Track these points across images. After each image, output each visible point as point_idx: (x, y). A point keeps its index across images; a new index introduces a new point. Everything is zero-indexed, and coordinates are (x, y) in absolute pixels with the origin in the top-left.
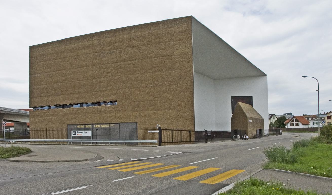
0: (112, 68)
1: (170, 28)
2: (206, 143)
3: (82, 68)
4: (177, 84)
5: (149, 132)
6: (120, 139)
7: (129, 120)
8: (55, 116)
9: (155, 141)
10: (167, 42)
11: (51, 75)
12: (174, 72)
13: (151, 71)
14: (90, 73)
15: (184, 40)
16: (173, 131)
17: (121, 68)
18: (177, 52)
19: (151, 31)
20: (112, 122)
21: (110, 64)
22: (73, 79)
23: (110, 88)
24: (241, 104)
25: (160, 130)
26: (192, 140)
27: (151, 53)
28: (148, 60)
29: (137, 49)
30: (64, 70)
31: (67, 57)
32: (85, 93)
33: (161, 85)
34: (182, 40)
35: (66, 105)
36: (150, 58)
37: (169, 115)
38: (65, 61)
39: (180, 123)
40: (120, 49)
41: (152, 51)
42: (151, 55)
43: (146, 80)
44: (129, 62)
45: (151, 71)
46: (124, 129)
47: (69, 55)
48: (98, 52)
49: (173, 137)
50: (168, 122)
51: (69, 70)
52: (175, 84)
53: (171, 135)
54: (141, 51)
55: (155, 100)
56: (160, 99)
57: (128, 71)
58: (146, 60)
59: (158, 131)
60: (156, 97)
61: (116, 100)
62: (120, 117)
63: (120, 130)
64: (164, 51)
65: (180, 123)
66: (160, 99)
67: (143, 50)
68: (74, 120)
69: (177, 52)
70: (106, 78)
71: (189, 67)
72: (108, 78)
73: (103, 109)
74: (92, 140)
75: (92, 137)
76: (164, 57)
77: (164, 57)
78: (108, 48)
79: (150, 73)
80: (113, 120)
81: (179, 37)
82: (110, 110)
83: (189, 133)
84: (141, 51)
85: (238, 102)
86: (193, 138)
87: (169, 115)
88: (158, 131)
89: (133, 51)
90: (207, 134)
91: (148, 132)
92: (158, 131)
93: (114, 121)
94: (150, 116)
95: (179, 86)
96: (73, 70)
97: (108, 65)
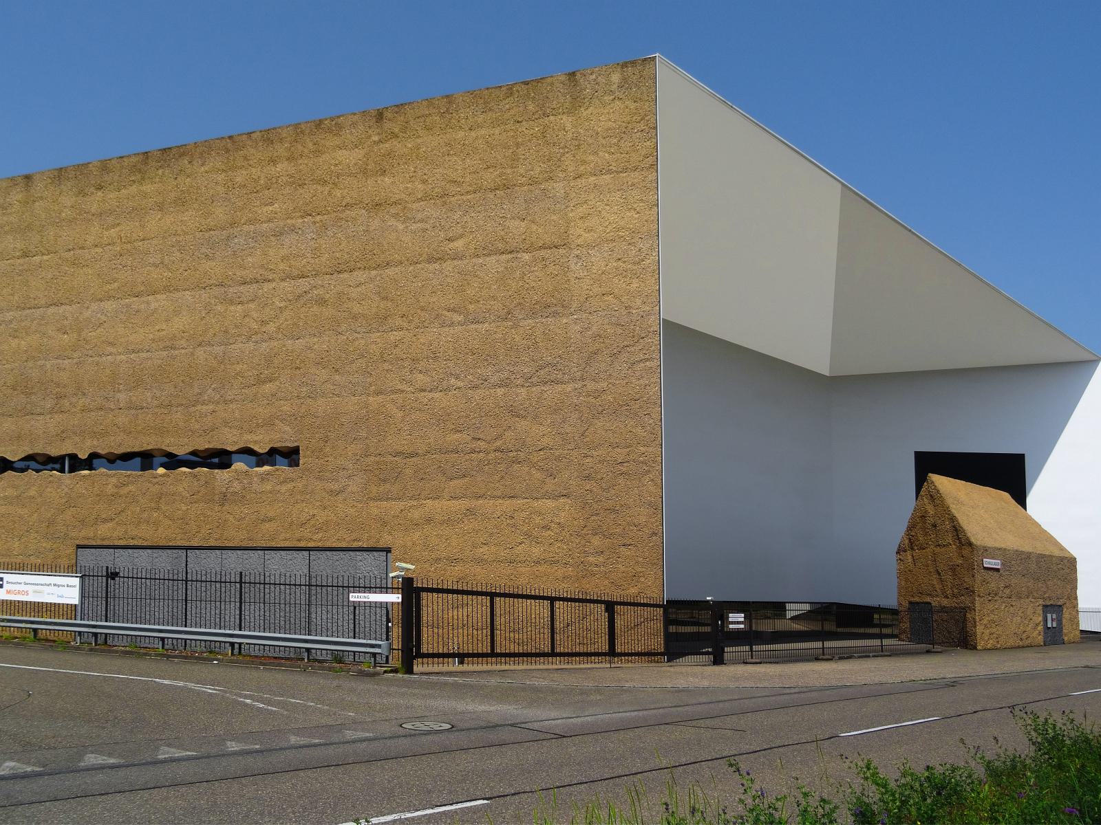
0: (282, 300)
1: (552, 118)
2: (718, 660)
3: (151, 298)
4: (583, 380)
5: (354, 597)
6: (117, 618)
7: (354, 536)
8: (24, 506)
9: (379, 646)
10: (533, 182)
11: (11, 322)
12: (565, 321)
13: (461, 318)
14: (179, 323)
15: (617, 172)
16: (557, 604)
17: (322, 302)
18: (581, 231)
19: (461, 134)
20: (274, 544)
21: (273, 280)
22: (112, 344)
23: (268, 388)
24: (942, 482)
25: (410, 589)
26: (353, 654)
27: (461, 236)
28: (445, 265)
29: (396, 216)
30: (71, 303)
31: (83, 248)
32: (160, 406)
33: (503, 384)
34: (609, 172)
35: (73, 457)
36: (457, 257)
37: (538, 520)
38: (74, 263)
39: (591, 559)
40: (318, 218)
41: (463, 227)
42: (459, 244)
43: (435, 358)
44: (360, 276)
45: (461, 318)
46: (238, 580)
47: (91, 240)
48: (223, 229)
49: (557, 624)
50: (536, 551)
51: (94, 306)
52: (574, 380)
53: (547, 613)
54: (414, 227)
55: (473, 451)
56: (498, 443)
57: (355, 317)
58: (437, 266)
59: (396, 598)
60: (481, 436)
61: (296, 444)
62: (312, 522)
63: (187, 581)
64: (523, 224)
65: (591, 559)
66: (498, 443)
67: (422, 221)
68: (110, 525)
69: (581, 231)
70: (251, 344)
71: (639, 302)
72: (264, 345)
73: (236, 483)
74: (78, 622)
75: (79, 608)
76: (519, 256)
77: (519, 256)
78: (265, 209)
79: (452, 324)
80: (282, 536)
81: (591, 158)
82: (269, 487)
83: (607, 610)
84: (414, 227)
85: (930, 475)
86: (651, 633)
87: (538, 520)
88: (396, 598)
89: (375, 223)
90: (724, 618)
91: (351, 599)
92: (400, 596)
93: (286, 540)
94: (448, 522)
95: (591, 386)
96: (109, 306)
97: (267, 287)
